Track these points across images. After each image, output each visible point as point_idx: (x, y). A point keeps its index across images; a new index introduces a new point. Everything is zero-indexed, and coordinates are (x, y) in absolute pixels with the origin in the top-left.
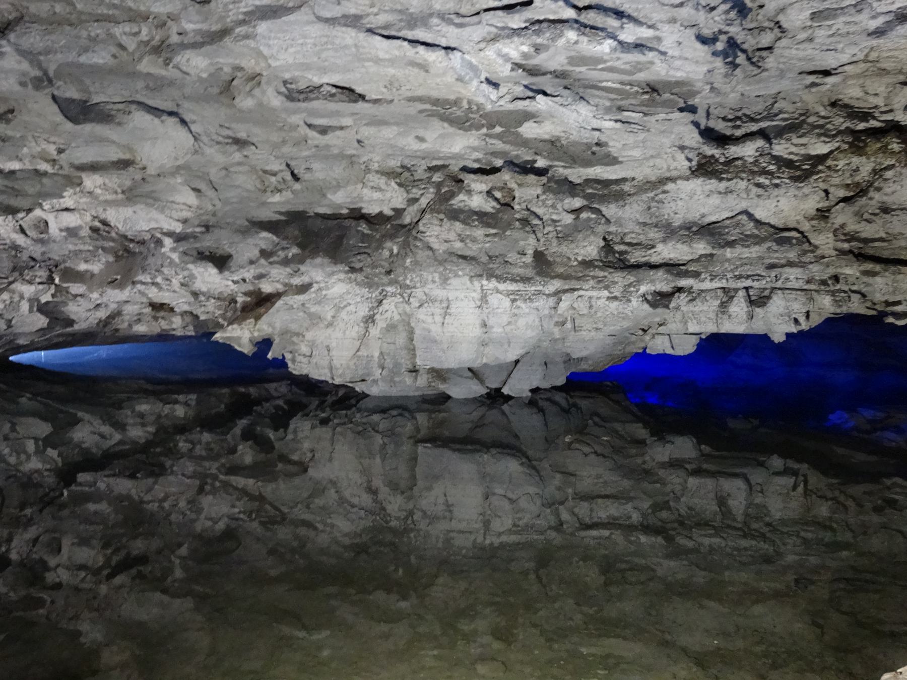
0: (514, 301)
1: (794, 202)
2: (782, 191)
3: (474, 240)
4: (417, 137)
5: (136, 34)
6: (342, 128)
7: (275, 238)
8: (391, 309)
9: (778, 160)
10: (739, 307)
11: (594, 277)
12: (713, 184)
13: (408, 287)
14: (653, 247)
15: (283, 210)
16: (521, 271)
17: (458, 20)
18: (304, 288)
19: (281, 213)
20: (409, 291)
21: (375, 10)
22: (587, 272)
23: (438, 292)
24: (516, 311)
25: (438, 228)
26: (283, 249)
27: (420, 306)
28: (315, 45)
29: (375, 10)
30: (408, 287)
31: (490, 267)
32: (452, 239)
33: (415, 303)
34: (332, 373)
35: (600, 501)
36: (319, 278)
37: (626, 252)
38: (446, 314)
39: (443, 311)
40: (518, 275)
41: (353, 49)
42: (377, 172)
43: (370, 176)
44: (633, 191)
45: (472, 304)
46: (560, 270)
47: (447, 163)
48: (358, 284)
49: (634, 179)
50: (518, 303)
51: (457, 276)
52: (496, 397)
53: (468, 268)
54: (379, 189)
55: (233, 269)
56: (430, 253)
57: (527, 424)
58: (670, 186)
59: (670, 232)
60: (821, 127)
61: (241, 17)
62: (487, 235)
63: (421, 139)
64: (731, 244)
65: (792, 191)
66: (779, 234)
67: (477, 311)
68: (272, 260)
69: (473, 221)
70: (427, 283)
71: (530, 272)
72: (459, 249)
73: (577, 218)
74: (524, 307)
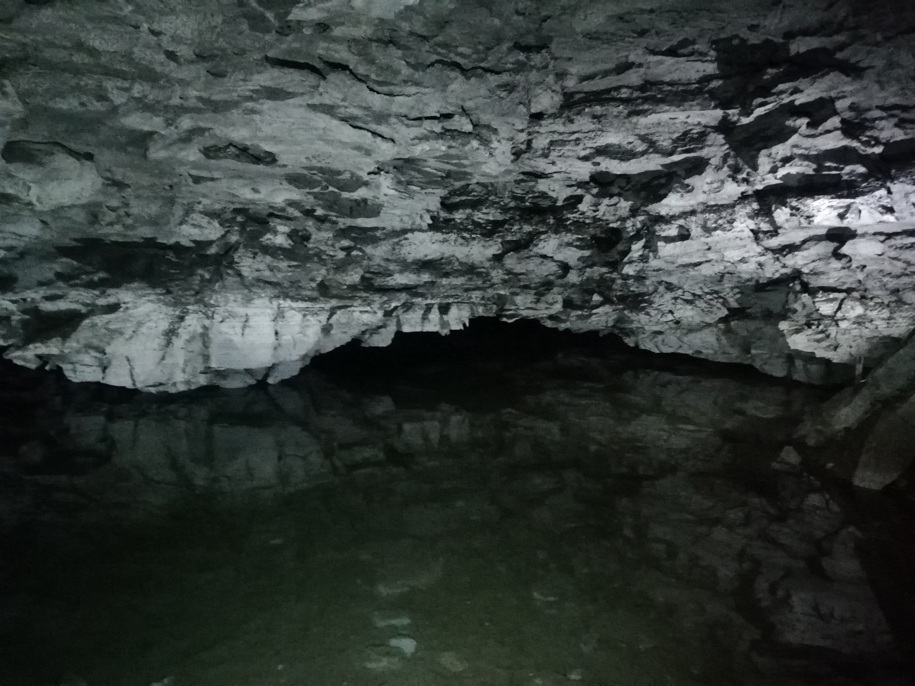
0: (305, 316)
1: (482, 249)
2: (475, 242)
3: (279, 270)
4: (253, 189)
5: (126, 90)
6: (212, 179)
7: (75, 263)
8: (193, 322)
9: (475, 223)
10: (434, 315)
11: (360, 297)
12: (439, 236)
13: (213, 306)
14: (390, 275)
15: (78, 237)
16: (309, 293)
17: (407, 122)
18: (113, 308)
19: (75, 240)
20: (212, 309)
21: (346, 104)
22: (355, 294)
23: (241, 311)
24: (307, 323)
25: (251, 260)
26: (86, 273)
27: (222, 322)
28: (293, 124)
29: (346, 104)
30: (213, 306)
31: (285, 290)
32: (262, 268)
33: (218, 318)
34: (134, 380)
35: (356, 448)
36: (126, 300)
37: (372, 279)
38: (244, 327)
39: (242, 324)
40: (307, 296)
41: (322, 131)
42: (201, 213)
43: (194, 216)
44: (382, 237)
45: (268, 319)
46: (335, 292)
47: (247, 207)
48: (166, 304)
49: (384, 228)
50: (308, 317)
51: (260, 297)
52: (262, 384)
53: (270, 291)
54: (200, 227)
55: (17, 290)
56: (238, 279)
57: (292, 403)
58: (409, 235)
59: (405, 266)
60: (498, 203)
61: (248, 93)
62: (290, 266)
63: (255, 191)
64: (447, 275)
65: (482, 242)
66: (470, 270)
67: (272, 323)
68: (71, 282)
69: (279, 255)
70: (228, 302)
71: (315, 294)
72: (268, 277)
73: (348, 255)
74: (312, 320)
